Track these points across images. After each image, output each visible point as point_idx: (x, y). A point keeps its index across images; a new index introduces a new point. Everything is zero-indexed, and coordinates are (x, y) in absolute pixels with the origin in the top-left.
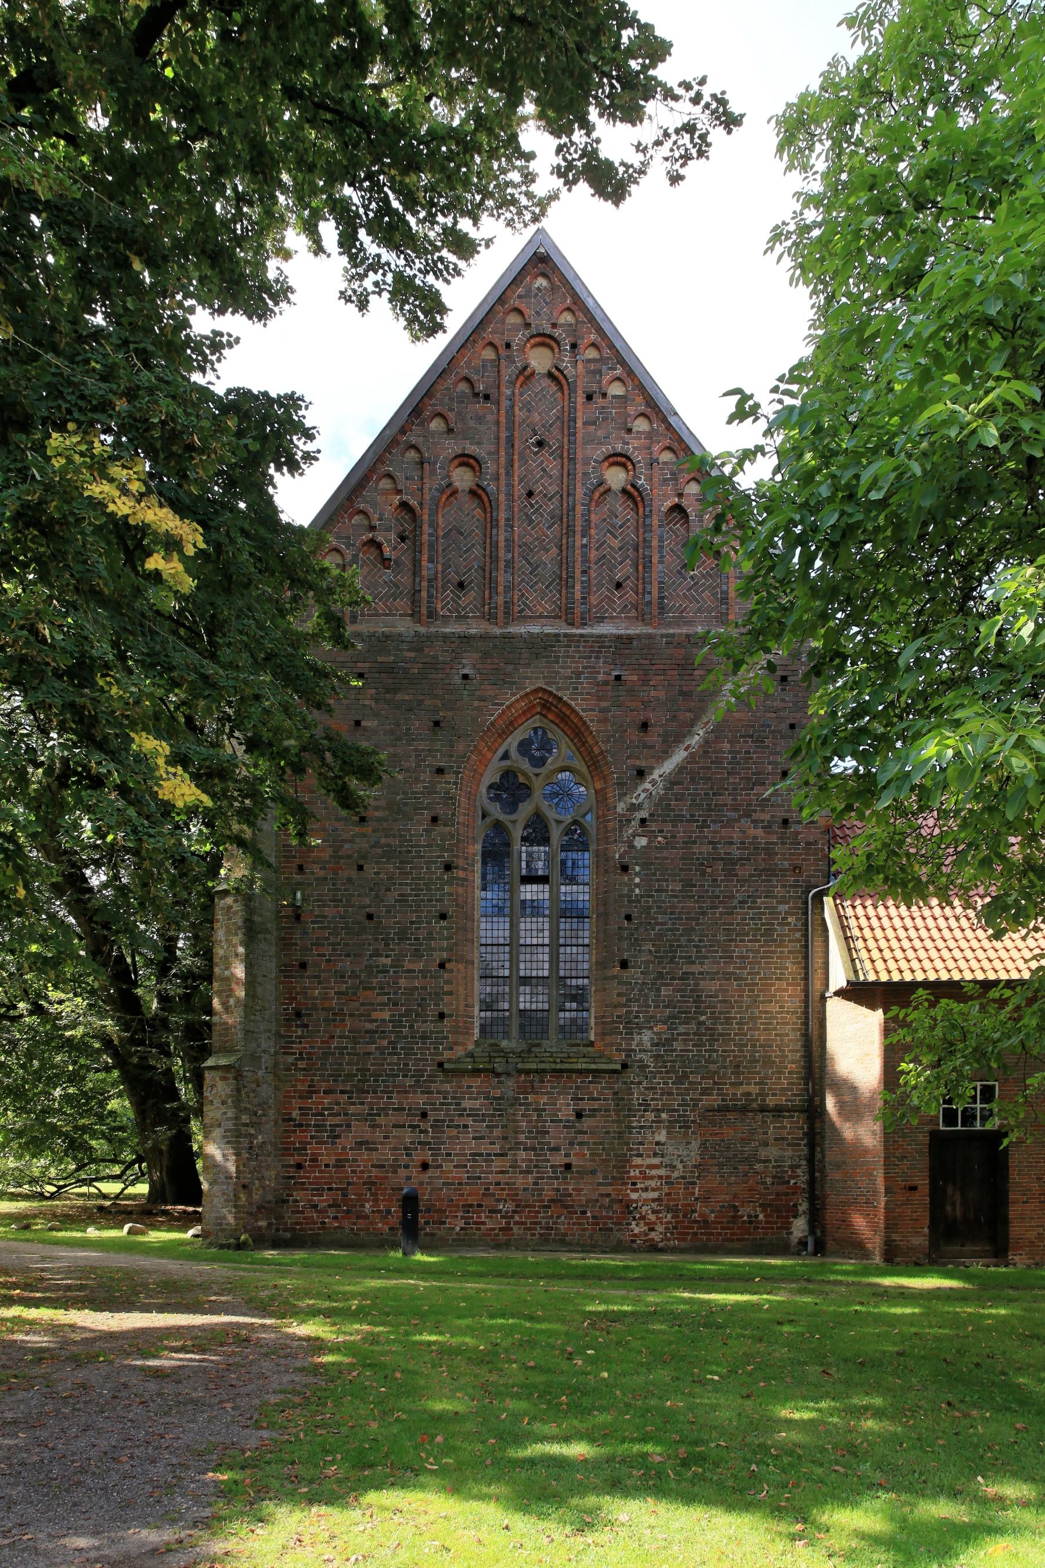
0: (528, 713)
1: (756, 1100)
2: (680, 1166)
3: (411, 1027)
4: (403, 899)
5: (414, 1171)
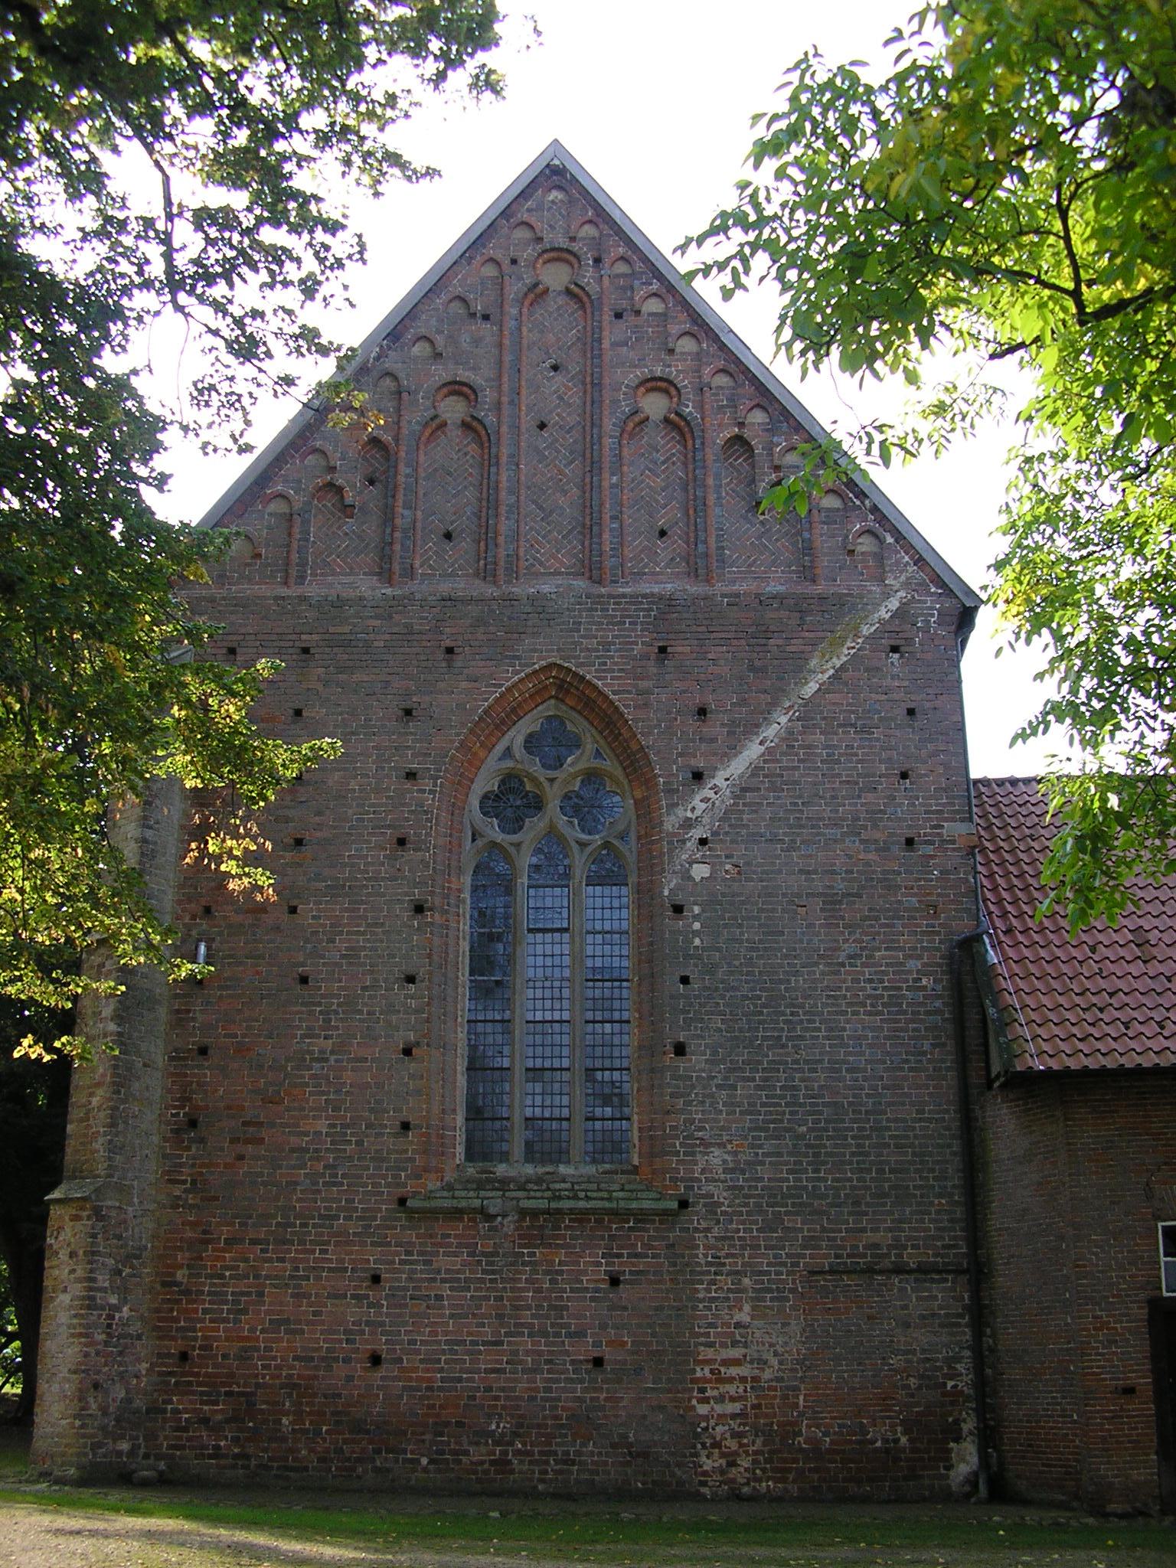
0: (538, 695)
1: (888, 1255)
2: (774, 1362)
3: (359, 1143)
4: (352, 954)
5: (359, 1368)
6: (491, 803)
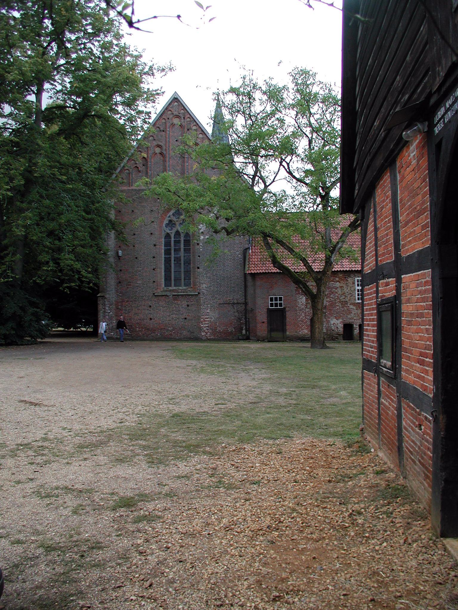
4: (144, 253)
6: (167, 225)
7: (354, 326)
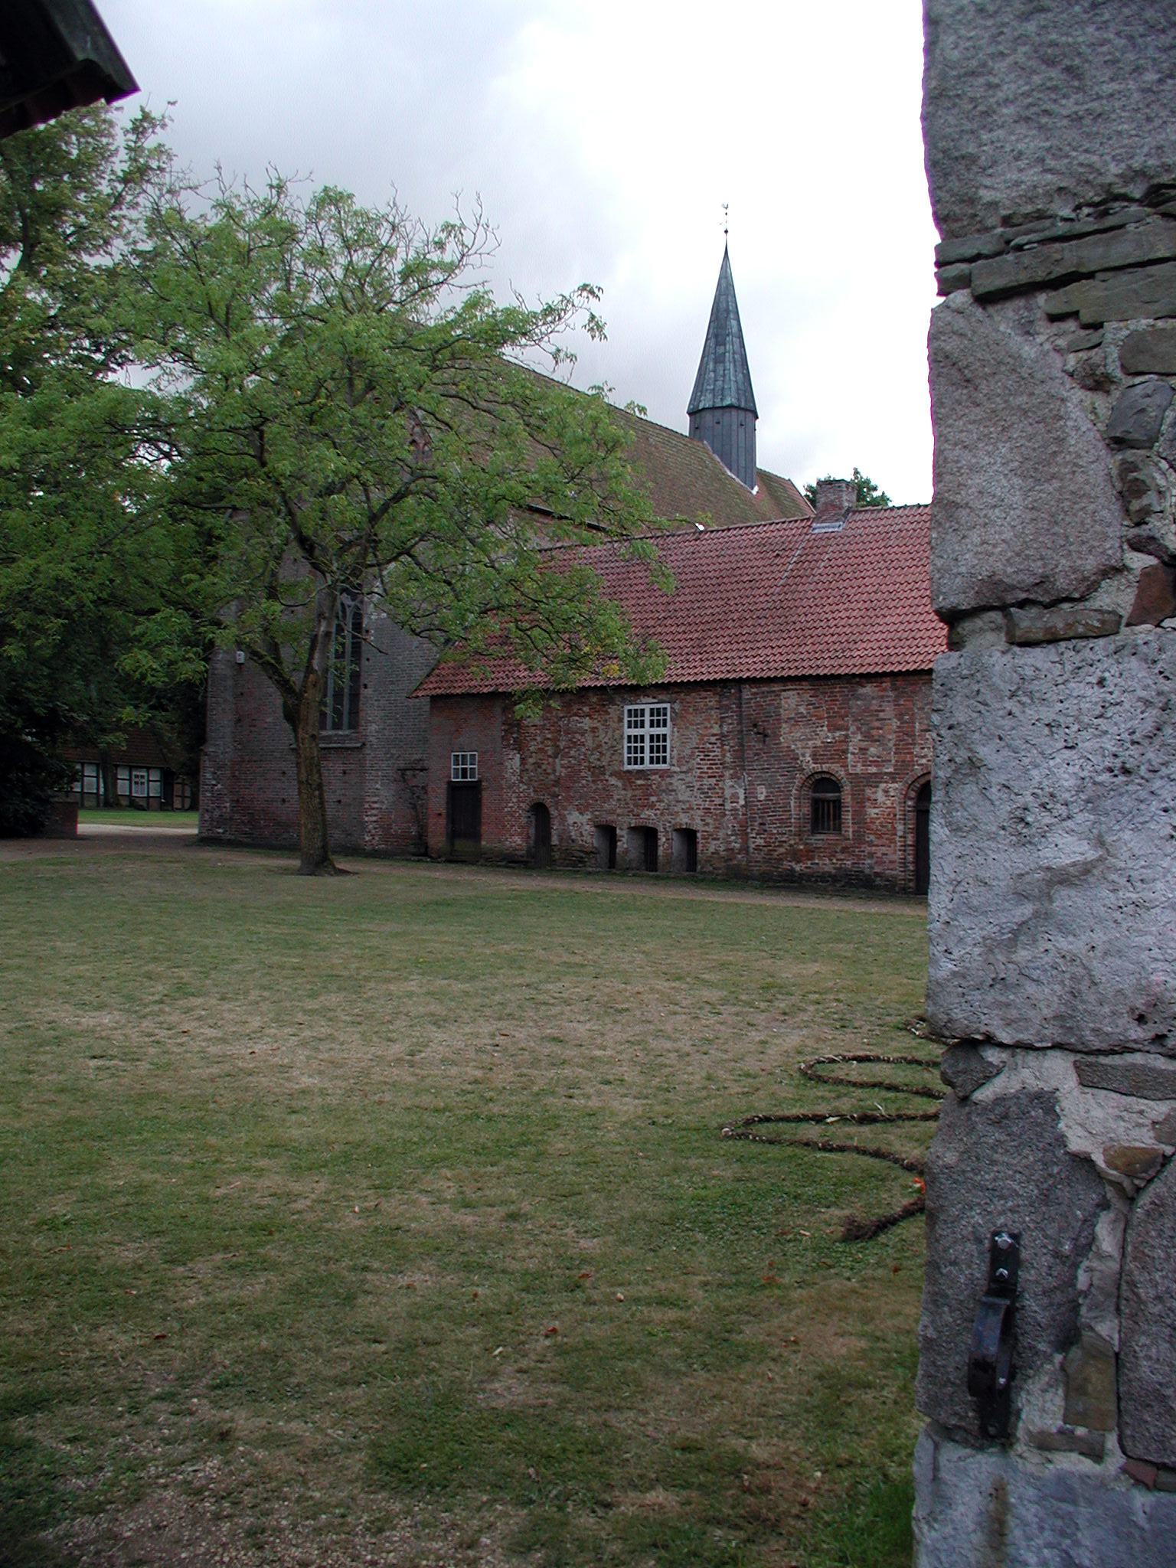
7: (618, 831)
